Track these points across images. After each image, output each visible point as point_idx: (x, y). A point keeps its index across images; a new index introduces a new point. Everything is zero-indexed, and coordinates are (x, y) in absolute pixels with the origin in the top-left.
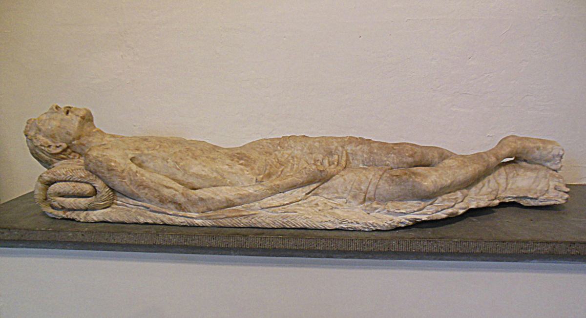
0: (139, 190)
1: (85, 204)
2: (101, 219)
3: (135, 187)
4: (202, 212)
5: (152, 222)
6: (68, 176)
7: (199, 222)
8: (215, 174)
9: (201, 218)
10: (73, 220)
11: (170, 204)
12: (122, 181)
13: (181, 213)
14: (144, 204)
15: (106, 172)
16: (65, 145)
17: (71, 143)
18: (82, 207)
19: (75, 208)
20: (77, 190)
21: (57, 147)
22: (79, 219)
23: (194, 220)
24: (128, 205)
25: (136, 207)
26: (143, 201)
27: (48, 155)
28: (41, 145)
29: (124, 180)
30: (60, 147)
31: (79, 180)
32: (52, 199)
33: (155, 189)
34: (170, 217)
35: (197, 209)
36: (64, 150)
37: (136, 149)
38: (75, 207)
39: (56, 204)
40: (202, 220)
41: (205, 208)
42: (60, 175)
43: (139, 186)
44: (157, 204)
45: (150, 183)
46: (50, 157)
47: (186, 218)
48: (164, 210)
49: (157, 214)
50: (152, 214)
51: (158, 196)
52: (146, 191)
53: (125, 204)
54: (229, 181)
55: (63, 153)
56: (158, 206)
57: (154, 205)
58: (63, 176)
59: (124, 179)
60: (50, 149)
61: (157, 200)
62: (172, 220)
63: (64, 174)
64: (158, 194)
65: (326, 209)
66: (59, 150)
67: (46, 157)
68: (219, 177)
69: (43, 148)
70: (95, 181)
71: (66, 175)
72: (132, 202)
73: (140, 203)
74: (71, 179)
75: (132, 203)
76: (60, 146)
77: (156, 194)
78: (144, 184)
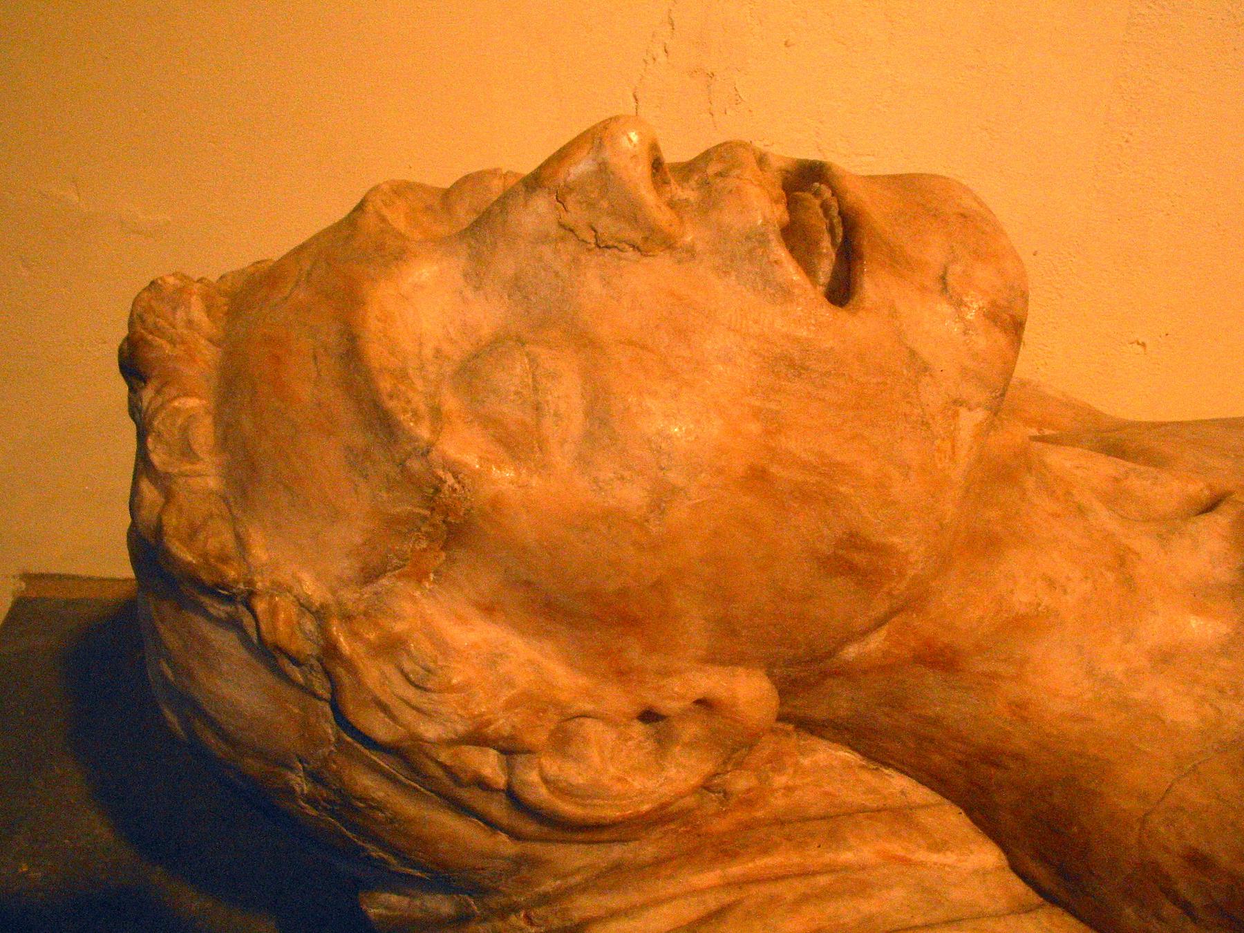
60: (573, 774)
69: (489, 764)
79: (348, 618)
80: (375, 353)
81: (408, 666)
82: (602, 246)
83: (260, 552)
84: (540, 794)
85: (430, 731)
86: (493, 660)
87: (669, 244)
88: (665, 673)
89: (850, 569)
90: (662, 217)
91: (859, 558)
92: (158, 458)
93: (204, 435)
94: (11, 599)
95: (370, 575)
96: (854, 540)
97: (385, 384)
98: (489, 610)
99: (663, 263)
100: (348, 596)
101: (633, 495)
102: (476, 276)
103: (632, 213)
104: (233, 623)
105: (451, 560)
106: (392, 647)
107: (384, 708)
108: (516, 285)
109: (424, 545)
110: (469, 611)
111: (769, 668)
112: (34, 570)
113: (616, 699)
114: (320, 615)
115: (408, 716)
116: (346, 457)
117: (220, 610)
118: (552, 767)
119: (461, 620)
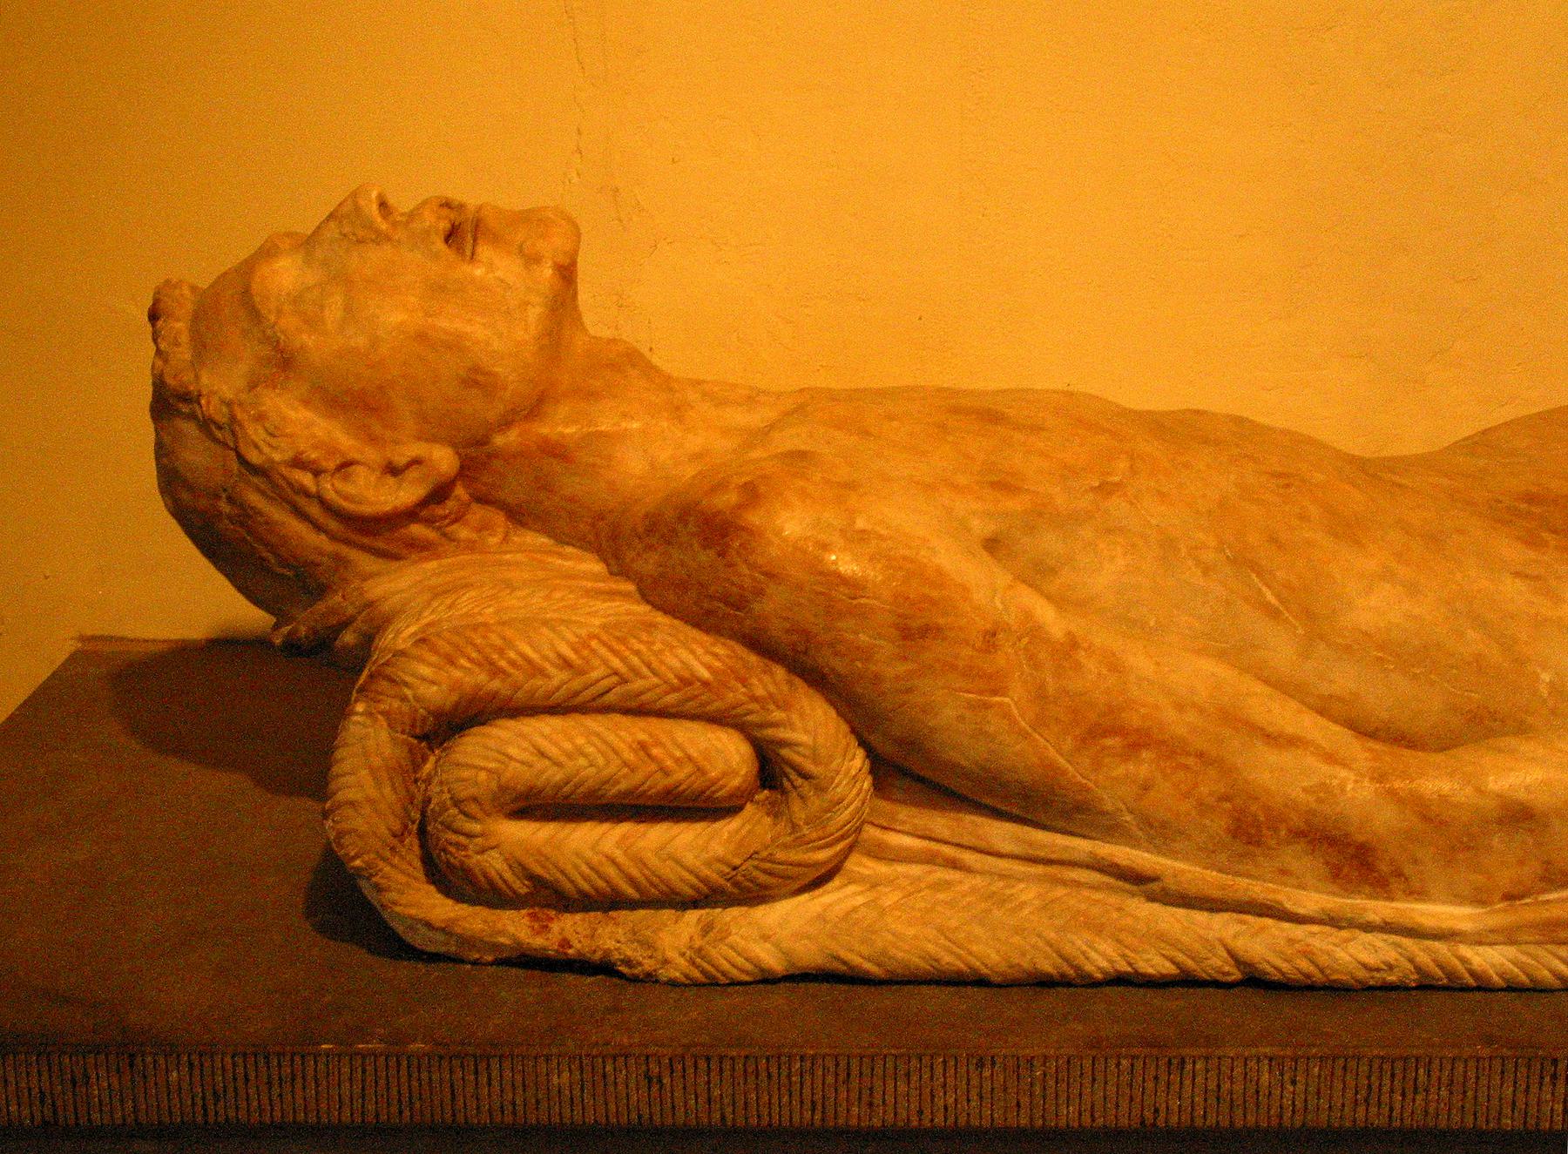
0: (1097, 765)
1: (708, 864)
2: (809, 954)
3: (1069, 743)
4: (1509, 897)
5: (1169, 968)
6: (595, 675)
7: (1491, 960)
8: (1474, 640)
9: (1509, 936)
10: (604, 968)
11: (1300, 847)
12: (987, 706)
13: (1378, 909)
14: (1123, 854)
15: (886, 648)
16: (444, 459)
17: (482, 442)
18: (684, 883)
19: (630, 891)
20: (666, 773)
21: (393, 470)
22: (649, 965)
23: (1465, 951)
24: (969, 857)
25: (1039, 869)
26: (1112, 830)
27: (333, 525)
28: (298, 463)
29: (997, 699)
30: (413, 474)
31: (671, 698)
32: (470, 836)
33: (1200, 755)
34: (1298, 931)
35: (1479, 879)
36: (439, 494)
37: (1280, 547)
38: (632, 881)
39: (494, 864)
40: (1511, 951)
41: (1531, 869)
42: (536, 670)
43: (1095, 733)
44: (1207, 854)
45: (1170, 714)
46: (333, 537)
47: (1407, 942)
48: (1258, 890)
49: (1201, 917)
50: (1172, 919)
51: (1226, 798)
52: (1144, 766)
53: (947, 850)
54: (1546, 677)
55: (424, 513)
56: (1212, 867)
57: (1186, 858)
58: (559, 676)
59: (995, 692)
60: (349, 489)
61: (1218, 825)
62: (1307, 954)
63: (567, 664)
64: (1221, 788)
65: (1123, 807)
66: (405, 494)
67: (321, 541)
68: (1494, 654)
69: (306, 479)
70: (785, 706)
71: (581, 672)
72: (1018, 840)
73: (1081, 846)
74: (610, 698)
75: (1007, 847)
76: (416, 462)
77: (1209, 786)
78: (1133, 719)
79: (240, 405)
80: (255, 287)
81: (267, 425)
82: (359, 242)
83: (205, 380)
84: (330, 495)
85: (277, 457)
86: (309, 425)
87: (389, 239)
88: (396, 442)
89: (476, 383)
90: (384, 226)
91: (480, 378)
92: (163, 346)
93: (184, 338)
94: (70, 647)
95: (252, 386)
96: (476, 369)
97: (257, 299)
98: (306, 403)
99: (387, 247)
100: (243, 396)
101: (361, 341)
102: (308, 262)
103: (370, 226)
104: (192, 417)
105: (287, 378)
106: (260, 418)
107: (256, 446)
108: (325, 263)
109: (275, 370)
110: (296, 404)
111: (453, 445)
112: (89, 633)
113: (372, 454)
114: (229, 404)
115: (266, 450)
116: (395, 571)
117: (185, 409)
118: (339, 485)
119: (294, 409)
